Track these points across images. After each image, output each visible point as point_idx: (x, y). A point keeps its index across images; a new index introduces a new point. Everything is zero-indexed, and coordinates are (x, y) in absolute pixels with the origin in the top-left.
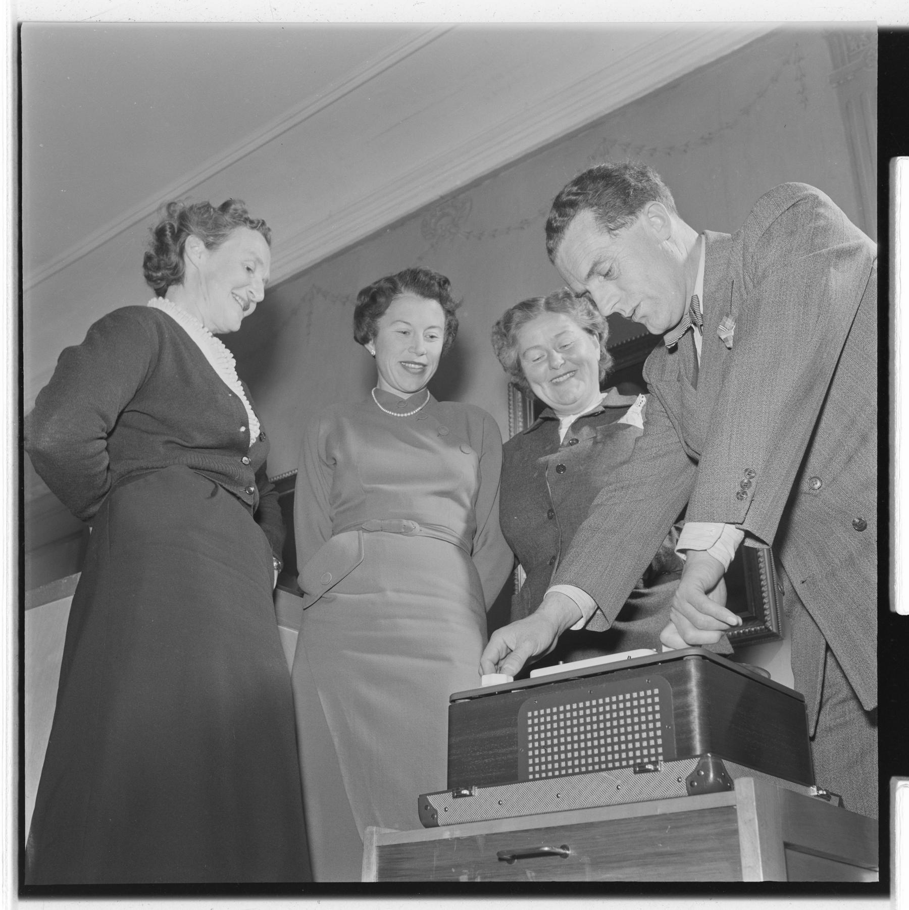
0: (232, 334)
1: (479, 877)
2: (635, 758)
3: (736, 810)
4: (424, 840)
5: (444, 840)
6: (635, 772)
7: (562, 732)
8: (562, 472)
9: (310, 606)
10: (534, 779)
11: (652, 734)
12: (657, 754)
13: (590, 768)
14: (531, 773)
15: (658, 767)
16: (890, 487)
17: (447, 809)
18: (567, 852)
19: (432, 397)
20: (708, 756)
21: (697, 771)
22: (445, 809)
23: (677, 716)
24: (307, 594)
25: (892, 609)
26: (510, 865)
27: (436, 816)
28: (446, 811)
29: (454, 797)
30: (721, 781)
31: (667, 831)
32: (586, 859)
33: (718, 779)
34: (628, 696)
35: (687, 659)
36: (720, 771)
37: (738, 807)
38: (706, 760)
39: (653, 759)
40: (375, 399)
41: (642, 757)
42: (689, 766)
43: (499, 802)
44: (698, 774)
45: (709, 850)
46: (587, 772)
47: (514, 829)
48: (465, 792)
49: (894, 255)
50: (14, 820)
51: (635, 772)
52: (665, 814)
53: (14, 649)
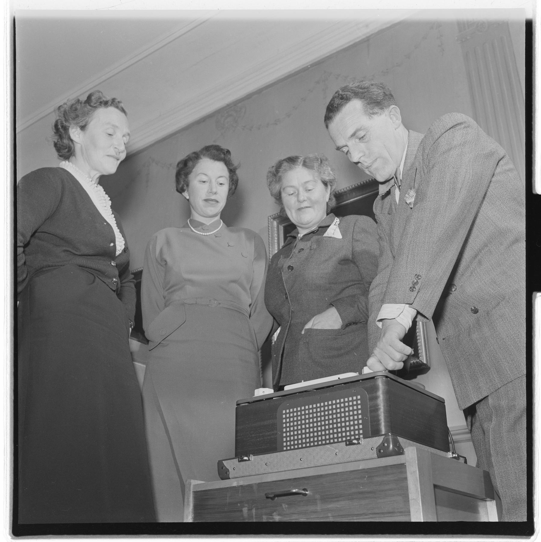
1: (254, 508)
2: (346, 436)
3: (406, 466)
4: (221, 487)
5: (234, 487)
6: (347, 445)
7: (303, 422)
8: (290, 270)
9: (153, 349)
10: (287, 450)
11: (356, 422)
12: (359, 434)
13: (320, 443)
14: (285, 446)
15: (360, 441)
17: (235, 469)
18: (307, 493)
19: (224, 224)
20: (389, 435)
21: (383, 444)
22: (234, 468)
23: (371, 411)
24: (151, 341)
26: (273, 501)
27: (228, 473)
28: (234, 470)
29: (239, 461)
30: (397, 449)
31: (365, 479)
32: (318, 496)
33: (395, 448)
34: (342, 400)
35: (377, 378)
36: (396, 442)
37: (407, 464)
38: (388, 437)
39: (357, 437)
40: (189, 225)
41: (350, 436)
42: (378, 441)
43: (266, 464)
44: (383, 445)
45: (391, 490)
46: (318, 445)
47: (274, 479)
48: (246, 458)
50: (11, 311)
51: (347, 445)
52: (364, 469)
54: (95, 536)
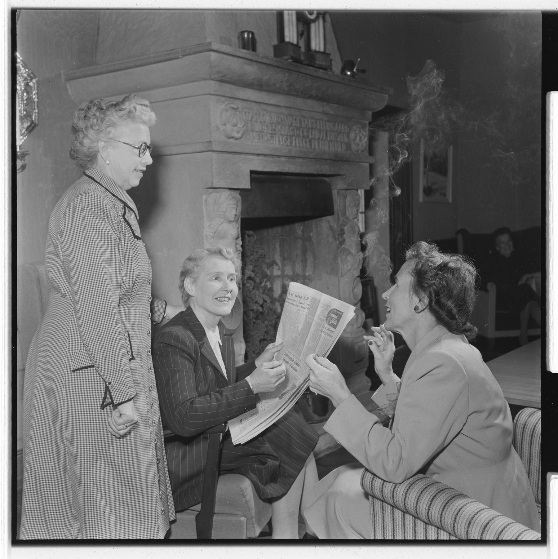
16: (547, 328)
25: (548, 370)
49: (549, 274)
50: (9, 499)
53: (9, 394)
54: (11, 419)
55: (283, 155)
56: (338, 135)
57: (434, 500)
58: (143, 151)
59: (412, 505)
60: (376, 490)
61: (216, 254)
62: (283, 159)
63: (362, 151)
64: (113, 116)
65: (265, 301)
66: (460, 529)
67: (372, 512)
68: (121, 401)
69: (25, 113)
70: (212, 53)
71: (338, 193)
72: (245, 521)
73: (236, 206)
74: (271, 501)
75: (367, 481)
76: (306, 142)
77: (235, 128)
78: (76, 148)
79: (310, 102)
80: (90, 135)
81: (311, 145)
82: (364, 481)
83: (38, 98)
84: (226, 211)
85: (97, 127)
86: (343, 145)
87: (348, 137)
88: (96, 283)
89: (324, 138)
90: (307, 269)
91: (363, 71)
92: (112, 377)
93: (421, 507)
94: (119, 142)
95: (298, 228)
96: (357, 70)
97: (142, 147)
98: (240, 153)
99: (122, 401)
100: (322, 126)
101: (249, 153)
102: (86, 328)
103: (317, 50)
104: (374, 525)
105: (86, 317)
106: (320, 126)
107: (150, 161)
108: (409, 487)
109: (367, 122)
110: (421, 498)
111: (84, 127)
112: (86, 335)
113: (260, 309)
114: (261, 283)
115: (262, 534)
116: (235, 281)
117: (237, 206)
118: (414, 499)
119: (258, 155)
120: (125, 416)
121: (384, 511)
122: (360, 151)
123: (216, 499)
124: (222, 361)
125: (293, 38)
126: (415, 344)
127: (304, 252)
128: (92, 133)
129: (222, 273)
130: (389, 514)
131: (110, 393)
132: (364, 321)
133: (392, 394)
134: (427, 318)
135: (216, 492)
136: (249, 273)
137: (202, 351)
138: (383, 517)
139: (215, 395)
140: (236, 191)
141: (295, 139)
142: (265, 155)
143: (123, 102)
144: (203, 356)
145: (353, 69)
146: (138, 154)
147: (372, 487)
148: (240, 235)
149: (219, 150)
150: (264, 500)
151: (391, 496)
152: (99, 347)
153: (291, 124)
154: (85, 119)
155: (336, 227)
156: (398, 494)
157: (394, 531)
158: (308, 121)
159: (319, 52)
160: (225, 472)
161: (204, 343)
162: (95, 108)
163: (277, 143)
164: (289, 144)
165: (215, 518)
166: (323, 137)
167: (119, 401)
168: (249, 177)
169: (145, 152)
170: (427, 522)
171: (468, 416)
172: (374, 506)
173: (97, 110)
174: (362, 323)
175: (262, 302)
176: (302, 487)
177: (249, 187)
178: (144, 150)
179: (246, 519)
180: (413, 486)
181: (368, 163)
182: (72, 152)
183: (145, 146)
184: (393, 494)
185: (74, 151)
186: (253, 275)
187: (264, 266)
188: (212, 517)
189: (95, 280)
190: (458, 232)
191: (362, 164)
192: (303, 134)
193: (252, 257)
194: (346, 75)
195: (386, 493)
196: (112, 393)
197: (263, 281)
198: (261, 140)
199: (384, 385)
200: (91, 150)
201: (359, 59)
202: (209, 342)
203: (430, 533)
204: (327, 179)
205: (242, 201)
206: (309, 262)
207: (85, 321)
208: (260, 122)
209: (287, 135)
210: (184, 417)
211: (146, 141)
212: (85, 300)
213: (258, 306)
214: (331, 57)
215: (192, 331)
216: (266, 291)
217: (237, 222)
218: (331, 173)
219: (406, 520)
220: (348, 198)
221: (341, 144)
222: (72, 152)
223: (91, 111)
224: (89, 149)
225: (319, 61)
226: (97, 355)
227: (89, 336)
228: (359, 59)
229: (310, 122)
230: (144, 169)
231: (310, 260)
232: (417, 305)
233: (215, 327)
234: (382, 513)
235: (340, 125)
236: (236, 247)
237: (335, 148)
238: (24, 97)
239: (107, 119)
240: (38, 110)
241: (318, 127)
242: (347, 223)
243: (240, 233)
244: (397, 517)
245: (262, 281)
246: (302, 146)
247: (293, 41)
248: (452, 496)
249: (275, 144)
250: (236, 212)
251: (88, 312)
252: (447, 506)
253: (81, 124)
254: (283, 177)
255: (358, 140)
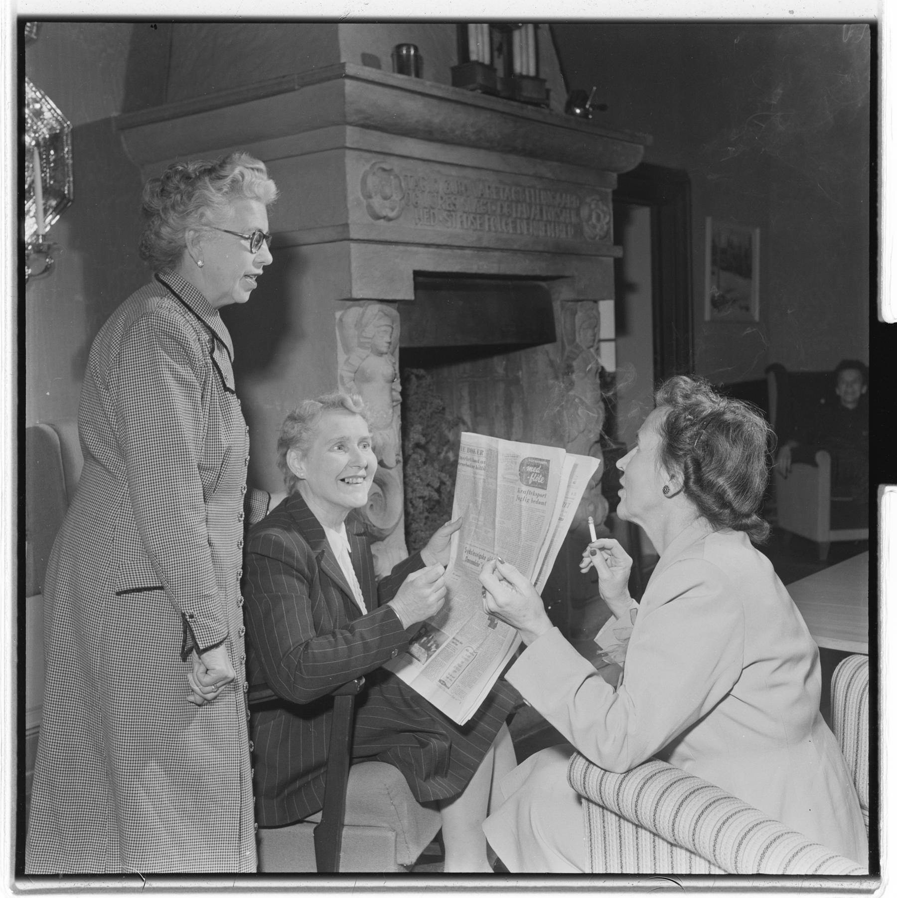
0: (236, 306)
25: (880, 320)
54: (879, 509)
55: (468, 245)
56: (561, 211)
57: (684, 806)
58: (256, 243)
59: (648, 813)
60: (591, 789)
61: (337, 407)
62: (468, 252)
63: (602, 238)
64: (212, 192)
65: (443, 483)
66: (725, 854)
67: (587, 825)
68: (209, 644)
69: (52, 182)
70: (348, 82)
71: (562, 307)
72: (393, 838)
73: (390, 329)
74: (438, 805)
75: (578, 775)
76: (507, 224)
77: (387, 203)
78: (149, 242)
79: (513, 158)
80: (171, 221)
81: (515, 228)
82: (572, 774)
83: (73, 158)
84: (374, 336)
85: (182, 207)
86: (569, 228)
87: (578, 214)
88: (173, 457)
89: (538, 217)
90: (514, 430)
91: (603, 108)
92: (195, 607)
93: (661, 817)
94: (217, 231)
95: (499, 364)
96: (591, 106)
97: (256, 237)
98: (396, 243)
99: (211, 644)
100: (533, 199)
101: (411, 242)
102: (155, 528)
103: (524, 73)
104: (591, 846)
105: (155, 510)
106: (530, 198)
107: (269, 259)
108: (644, 784)
109: (610, 191)
110: (662, 802)
111: (160, 208)
112: (155, 540)
113: (436, 496)
114: (439, 453)
115: (423, 859)
116: (370, 447)
117: (393, 328)
118: (651, 803)
119: (427, 245)
120: (213, 671)
121: (606, 823)
122: (598, 238)
123: (347, 803)
124: (355, 577)
125: (483, 55)
126: (665, 546)
127: (509, 402)
128: (174, 217)
129: (348, 439)
130: (614, 827)
131: (191, 631)
132: (606, 515)
133: (623, 628)
134: (683, 507)
135: (346, 793)
136: (416, 436)
137: (322, 565)
138: (604, 832)
139: (342, 634)
140: (391, 304)
141: (489, 219)
142: (438, 246)
143: (222, 165)
144: (324, 572)
145: (585, 104)
146: (249, 248)
147: (584, 783)
148: (398, 375)
149: (361, 237)
150: (425, 805)
151: (616, 799)
152: (175, 559)
153: (482, 195)
154: (162, 196)
155: (559, 362)
156: (625, 796)
157: (621, 857)
158: (510, 190)
159: (527, 77)
160: (361, 759)
161: (323, 551)
162: (178, 177)
163: (459, 226)
164: (478, 227)
165: (345, 832)
166: (535, 215)
167: (206, 645)
168: (412, 282)
169: (260, 245)
170: (672, 842)
171: (743, 669)
172: (589, 815)
173: (181, 180)
174: (603, 517)
175: (438, 484)
176: (490, 782)
177: (412, 298)
178: (258, 241)
179: (394, 833)
180: (650, 782)
181: (610, 256)
182: (143, 249)
183: (260, 235)
184: (618, 794)
185: (146, 247)
186: (423, 441)
187: (444, 426)
188: (341, 831)
189: (172, 452)
190: (768, 370)
191: (601, 258)
192: (501, 211)
193: (423, 411)
194: (574, 114)
195: (607, 794)
196: (195, 632)
197: (442, 450)
198: (432, 222)
199: (617, 618)
200: (173, 244)
201: (595, 88)
202: (330, 548)
203: (679, 860)
204: (543, 284)
205: (401, 320)
206: (516, 418)
207: (153, 517)
208: (429, 192)
209: (476, 213)
210: (296, 670)
211: (260, 227)
212: (155, 484)
213: (432, 491)
214: (548, 85)
215: (302, 533)
216: (447, 467)
217: (392, 354)
218: (550, 274)
219: (640, 839)
220: (579, 314)
221: (567, 227)
222: (143, 249)
223: (172, 181)
224: (170, 243)
225: (529, 91)
226: (171, 572)
227: (160, 542)
228: (595, 88)
229: (513, 191)
230: (260, 272)
231: (518, 416)
232: (667, 483)
233: (340, 524)
234: (602, 827)
235: (564, 196)
236: (392, 396)
237: (555, 233)
238: (50, 157)
239: (197, 194)
240: (74, 178)
241: (528, 200)
242: (578, 356)
243: (397, 372)
244: (626, 832)
245: (440, 451)
246: (500, 230)
247: (484, 58)
248: (713, 800)
249: (456, 228)
250: (391, 337)
251: (160, 504)
252: (703, 816)
253: (157, 204)
254: (478, 281)
255: (594, 220)
